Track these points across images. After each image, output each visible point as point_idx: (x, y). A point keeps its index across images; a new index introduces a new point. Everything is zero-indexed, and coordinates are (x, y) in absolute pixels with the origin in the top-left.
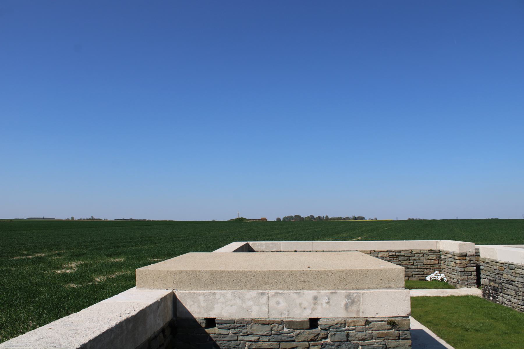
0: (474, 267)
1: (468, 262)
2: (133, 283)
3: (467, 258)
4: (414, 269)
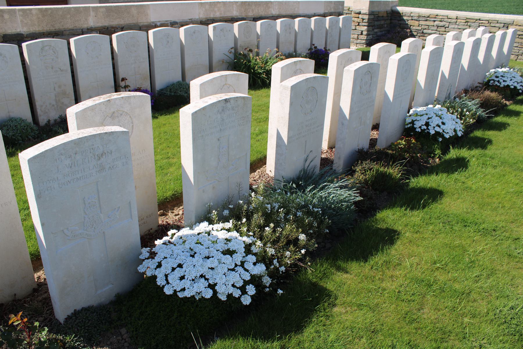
0: (365, 26)
1: (360, 20)
2: (173, 208)
3: (360, 16)
4: (449, 23)
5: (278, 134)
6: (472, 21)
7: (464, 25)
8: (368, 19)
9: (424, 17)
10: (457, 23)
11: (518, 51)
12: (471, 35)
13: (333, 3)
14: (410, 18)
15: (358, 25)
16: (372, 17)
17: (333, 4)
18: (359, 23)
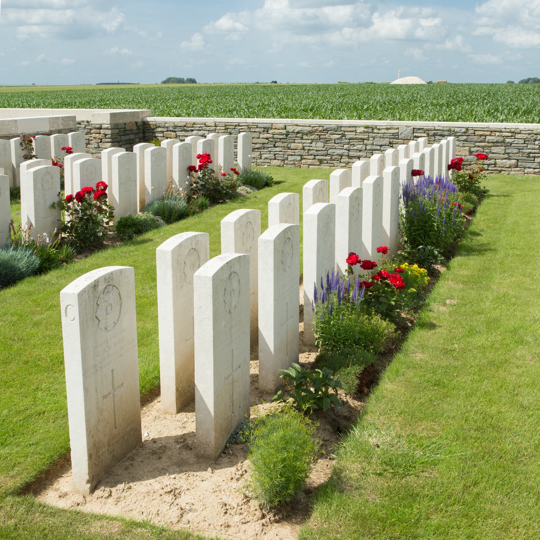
0: (108, 142)
3: (102, 131)
4: (208, 131)
5: (28, 219)
6: (231, 127)
7: (224, 132)
8: (111, 134)
9: (180, 126)
10: (217, 131)
11: (283, 156)
12: (345, 182)
13: (61, 119)
14: (165, 129)
15: (101, 142)
16: (117, 131)
17: (61, 120)
18: (101, 139)
